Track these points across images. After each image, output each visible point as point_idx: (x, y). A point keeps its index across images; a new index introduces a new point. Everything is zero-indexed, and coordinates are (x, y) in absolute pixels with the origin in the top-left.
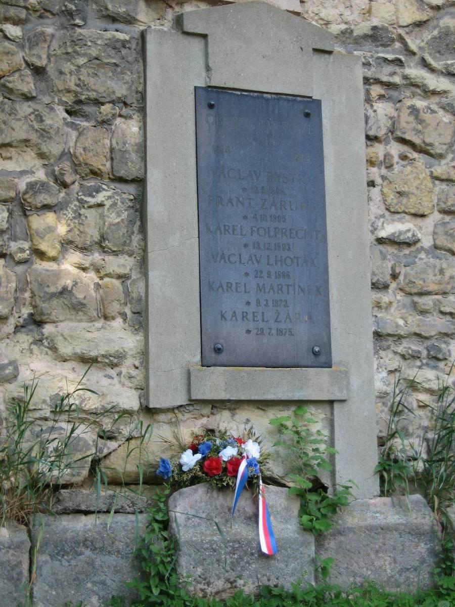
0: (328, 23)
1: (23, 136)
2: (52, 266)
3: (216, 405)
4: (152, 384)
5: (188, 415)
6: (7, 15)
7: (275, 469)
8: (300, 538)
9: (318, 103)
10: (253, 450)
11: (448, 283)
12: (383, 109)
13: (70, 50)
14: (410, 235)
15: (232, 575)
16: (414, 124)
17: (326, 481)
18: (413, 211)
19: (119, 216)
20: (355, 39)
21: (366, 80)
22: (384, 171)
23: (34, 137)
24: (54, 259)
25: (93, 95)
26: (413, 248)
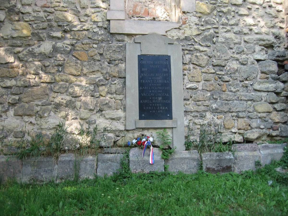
0: (173, 37)
1: (98, 69)
2: (104, 98)
3: (143, 129)
4: (127, 124)
5: (136, 131)
6: (94, 42)
7: (157, 143)
8: (161, 160)
9: (170, 56)
10: (151, 139)
11: (206, 98)
12: (188, 57)
13: (108, 49)
14: (195, 87)
15: (143, 168)
16: (196, 60)
17: (171, 147)
18: (196, 81)
19: (120, 86)
20: (181, 40)
21: (183, 50)
22: (188, 72)
23: (100, 69)
24: (104, 96)
25: (114, 59)
26: (196, 90)
